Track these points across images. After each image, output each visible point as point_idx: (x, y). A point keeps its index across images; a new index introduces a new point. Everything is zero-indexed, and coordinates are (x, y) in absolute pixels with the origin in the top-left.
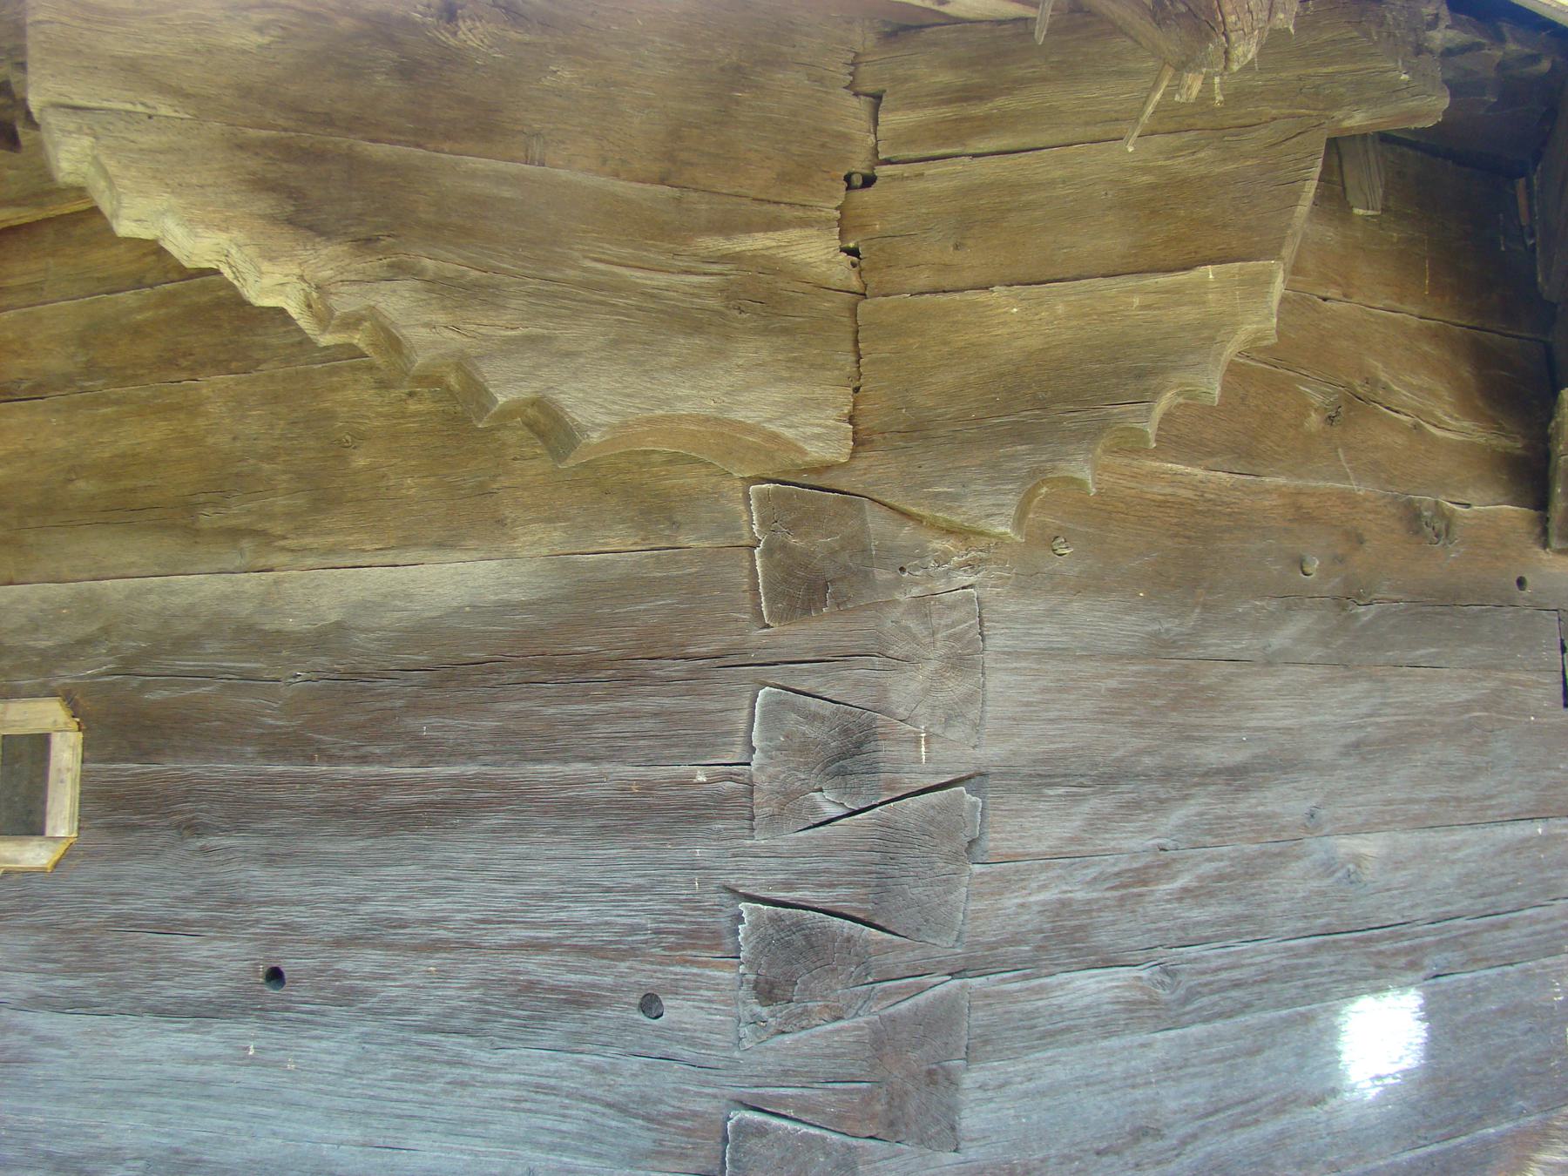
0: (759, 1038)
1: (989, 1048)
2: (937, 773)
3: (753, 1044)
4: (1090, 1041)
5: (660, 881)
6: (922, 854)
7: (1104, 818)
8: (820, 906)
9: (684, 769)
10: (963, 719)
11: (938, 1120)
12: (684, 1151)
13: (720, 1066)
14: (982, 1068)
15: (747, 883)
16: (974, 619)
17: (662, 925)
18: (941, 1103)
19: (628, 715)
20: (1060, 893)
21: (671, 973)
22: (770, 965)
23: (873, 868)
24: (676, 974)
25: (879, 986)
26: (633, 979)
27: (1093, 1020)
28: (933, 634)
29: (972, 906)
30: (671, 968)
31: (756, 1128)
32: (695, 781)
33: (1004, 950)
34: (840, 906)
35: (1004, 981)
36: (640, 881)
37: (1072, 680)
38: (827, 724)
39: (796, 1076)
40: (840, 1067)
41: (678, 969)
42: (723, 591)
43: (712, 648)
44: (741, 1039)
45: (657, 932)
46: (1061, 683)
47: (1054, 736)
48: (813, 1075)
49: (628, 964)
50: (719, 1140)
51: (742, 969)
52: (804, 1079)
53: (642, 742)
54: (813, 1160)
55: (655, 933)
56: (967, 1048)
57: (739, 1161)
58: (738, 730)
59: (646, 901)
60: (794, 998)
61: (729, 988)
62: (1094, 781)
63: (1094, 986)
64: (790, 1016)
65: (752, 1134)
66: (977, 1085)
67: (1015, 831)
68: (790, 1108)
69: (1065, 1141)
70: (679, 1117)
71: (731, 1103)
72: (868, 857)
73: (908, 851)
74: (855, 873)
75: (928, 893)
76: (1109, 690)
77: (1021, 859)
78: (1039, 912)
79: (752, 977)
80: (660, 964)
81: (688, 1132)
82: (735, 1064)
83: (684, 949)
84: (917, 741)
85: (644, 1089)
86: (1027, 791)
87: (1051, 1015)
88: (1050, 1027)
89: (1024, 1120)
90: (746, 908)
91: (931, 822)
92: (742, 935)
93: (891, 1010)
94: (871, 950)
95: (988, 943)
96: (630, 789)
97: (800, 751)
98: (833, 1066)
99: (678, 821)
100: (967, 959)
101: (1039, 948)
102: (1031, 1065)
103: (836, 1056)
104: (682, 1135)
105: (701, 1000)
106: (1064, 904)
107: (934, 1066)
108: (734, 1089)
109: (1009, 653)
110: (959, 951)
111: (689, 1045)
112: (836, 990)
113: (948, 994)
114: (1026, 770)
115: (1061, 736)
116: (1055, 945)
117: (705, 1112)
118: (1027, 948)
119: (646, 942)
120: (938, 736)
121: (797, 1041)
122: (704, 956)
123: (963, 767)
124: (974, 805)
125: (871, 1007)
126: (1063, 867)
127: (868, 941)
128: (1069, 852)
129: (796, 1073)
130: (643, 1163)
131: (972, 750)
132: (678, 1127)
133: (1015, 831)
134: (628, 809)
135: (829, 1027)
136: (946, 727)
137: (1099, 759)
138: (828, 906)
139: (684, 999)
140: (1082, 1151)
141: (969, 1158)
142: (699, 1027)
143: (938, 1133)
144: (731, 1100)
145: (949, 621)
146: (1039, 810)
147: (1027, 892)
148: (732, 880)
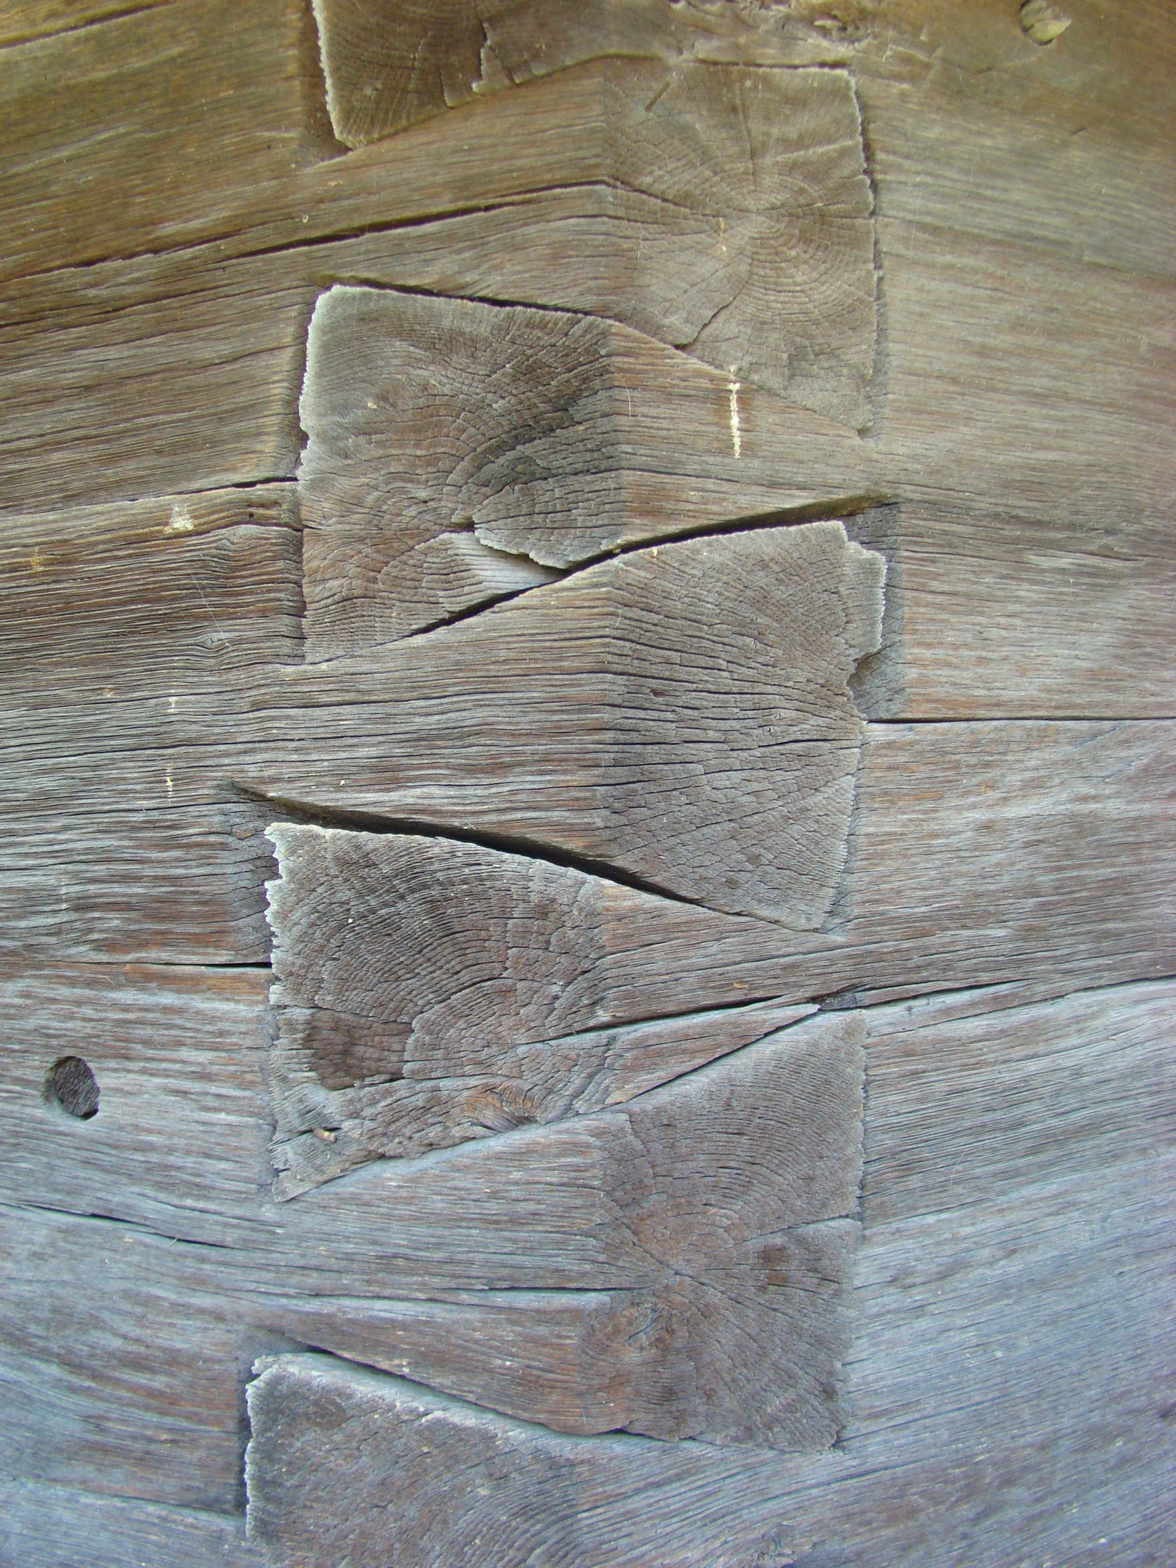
0: (319, 1169)
1: (914, 1182)
2: (773, 485)
3: (307, 1186)
4: (1143, 1151)
5: (88, 781)
6: (736, 686)
7: (1156, 634)
8: (468, 823)
9: (146, 502)
10: (833, 363)
11: (791, 1376)
12: (152, 1447)
13: (229, 1240)
14: (898, 1231)
15: (287, 772)
16: (852, 137)
17: (93, 888)
18: (794, 1329)
19: (29, 398)
20: (1071, 801)
21: (115, 1005)
22: (344, 984)
23: (606, 716)
24: (126, 1009)
25: (627, 1035)
26: (32, 1023)
27: (1146, 1102)
28: (753, 154)
29: (869, 825)
30: (115, 995)
31: (316, 1403)
32: (168, 530)
33: (947, 937)
34: (517, 822)
35: (949, 1014)
36: (47, 783)
37: (1076, 314)
38: (480, 355)
39: (410, 1272)
40: (529, 1250)
41: (127, 996)
42: (239, 86)
43: (217, 216)
44: (278, 1172)
45: (82, 905)
46: (1054, 318)
47: (1046, 433)
48: (458, 1270)
49: (20, 985)
50: (232, 1425)
51: (275, 993)
52: (436, 1281)
53: (56, 457)
54: (461, 1490)
55: (76, 909)
56: (862, 1187)
57: (275, 1483)
58: (266, 402)
59: (58, 831)
60: (407, 1068)
61: (248, 1042)
62: (1135, 545)
63: (1148, 1022)
64: (397, 1115)
65: (307, 1417)
66: (888, 1275)
67: (965, 645)
68: (403, 1354)
69: (1093, 1393)
70: (137, 1363)
71: (261, 1334)
72: (591, 686)
73: (702, 675)
74: (558, 732)
75: (755, 786)
76: (1154, 349)
77: (981, 713)
78: (1028, 844)
79: (300, 1014)
80: (90, 984)
81: (164, 1402)
82: (264, 1237)
83: (143, 945)
84: (720, 398)
85: (59, 1291)
86: (989, 551)
87: (1057, 1094)
88: (1055, 1122)
89: (999, 1354)
90: (283, 835)
91: (761, 602)
92: (274, 907)
93: (663, 1097)
94: (604, 936)
95: (909, 919)
96: (28, 566)
97: (416, 430)
98: (510, 1247)
99: (131, 629)
100: (859, 960)
101: (1028, 932)
102: (1012, 1217)
103: (515, 1221)
104: (147, 1408)
105: (181, 1074)
106: (1082, 826)
107: (778, 1240)
108: (263, 1300)
109: (936, 231)
110: (839, 938)
111: (159, 1186)
112: (514, 1046)
113: (813, 1050)
114: (983, 504)
115: (1060, 434)
116: (1065, 924)
117: (195, 1357)
118: (1002, 933)
119: (56, 931)
120: (771, 392)
121: (415, 1180)
122: (189, 961)
123: (836, 477)
124: (870, 570)
125: (607, 1092)
126: (1077, 740)
127: (593, 914)
128: (1090, 705)
129: (414, 1265)
130: (62, 1471)
131: (857, 441)
132: (134, 1388)
133: (965, 645)
134: (22, 613)
135: (498, 1144)
136: (792, 377)
137: (1144, 498)
138: (488, 822)
139: (143, 1071)
140: (1130, 1412)
141: (871, 1463)
142: (181, 1142)
143: (790, 1408)
144: (259, 1327)
145: (792, 132)
146: (1018, 600)
147: (998, 795)
148: (252, 769)
